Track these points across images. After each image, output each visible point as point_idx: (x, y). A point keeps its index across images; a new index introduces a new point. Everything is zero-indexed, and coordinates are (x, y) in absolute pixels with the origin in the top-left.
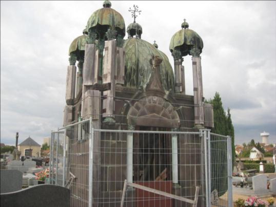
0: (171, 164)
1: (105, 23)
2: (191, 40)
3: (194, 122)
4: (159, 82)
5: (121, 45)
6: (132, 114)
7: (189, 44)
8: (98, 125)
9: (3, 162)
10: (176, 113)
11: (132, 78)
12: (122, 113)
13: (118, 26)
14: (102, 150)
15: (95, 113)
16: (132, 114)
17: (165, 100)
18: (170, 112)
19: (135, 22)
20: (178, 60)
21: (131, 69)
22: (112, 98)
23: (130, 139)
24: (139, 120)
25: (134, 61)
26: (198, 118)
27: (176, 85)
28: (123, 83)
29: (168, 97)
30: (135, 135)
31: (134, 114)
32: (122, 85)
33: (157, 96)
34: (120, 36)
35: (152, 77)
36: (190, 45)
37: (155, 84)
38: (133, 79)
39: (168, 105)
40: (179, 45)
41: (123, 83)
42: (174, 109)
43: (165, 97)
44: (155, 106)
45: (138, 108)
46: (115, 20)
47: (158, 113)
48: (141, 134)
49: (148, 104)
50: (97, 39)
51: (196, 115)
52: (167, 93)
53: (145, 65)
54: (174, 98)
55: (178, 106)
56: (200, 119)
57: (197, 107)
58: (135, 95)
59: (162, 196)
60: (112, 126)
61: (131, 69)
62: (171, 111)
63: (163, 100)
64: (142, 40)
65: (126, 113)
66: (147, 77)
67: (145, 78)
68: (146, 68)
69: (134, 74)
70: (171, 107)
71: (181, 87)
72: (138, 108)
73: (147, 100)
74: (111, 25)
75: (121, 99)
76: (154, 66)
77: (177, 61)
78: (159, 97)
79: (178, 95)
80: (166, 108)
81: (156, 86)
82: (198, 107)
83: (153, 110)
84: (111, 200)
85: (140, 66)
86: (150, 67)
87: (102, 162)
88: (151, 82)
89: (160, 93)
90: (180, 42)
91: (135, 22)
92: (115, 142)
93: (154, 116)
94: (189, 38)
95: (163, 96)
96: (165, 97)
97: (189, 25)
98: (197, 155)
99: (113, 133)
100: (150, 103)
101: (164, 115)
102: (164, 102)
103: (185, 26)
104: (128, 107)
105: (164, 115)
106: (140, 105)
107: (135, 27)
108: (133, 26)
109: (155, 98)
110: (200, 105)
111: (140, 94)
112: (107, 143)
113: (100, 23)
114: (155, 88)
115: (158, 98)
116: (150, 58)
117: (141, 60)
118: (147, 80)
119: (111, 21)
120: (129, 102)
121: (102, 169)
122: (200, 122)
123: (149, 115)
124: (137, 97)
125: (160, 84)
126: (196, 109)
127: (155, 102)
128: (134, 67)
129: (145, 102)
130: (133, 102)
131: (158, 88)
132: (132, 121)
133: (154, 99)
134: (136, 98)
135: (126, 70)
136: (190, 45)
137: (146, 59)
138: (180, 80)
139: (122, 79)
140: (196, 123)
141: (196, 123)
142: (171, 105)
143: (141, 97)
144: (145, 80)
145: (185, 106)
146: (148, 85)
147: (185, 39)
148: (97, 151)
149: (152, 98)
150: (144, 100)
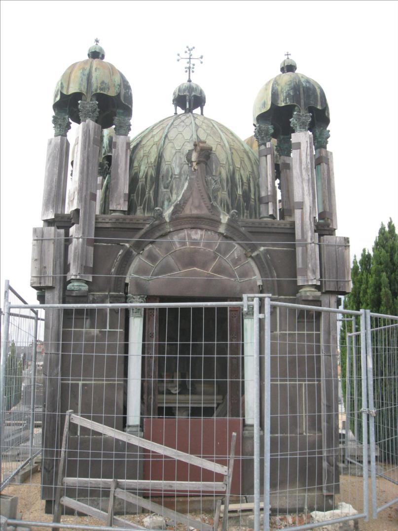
0: (243, 377)
1: (73, 89)
2: (288, 95)
3: (296, 282)
4: (205, 196)
5: (123, 132)
6: (136, 272)
7: (283, 104)
8: (56, 297)
9: (37, 426)
10: (253, 264)
11: (147, 196)
12: (113, 270)
13: (99, 91)
14: (65, 348)
15: (45, 273)
16: (136, 272)
17: (221, 234)
18: (235, 262)
19: (189, 81)
20: (265, 144)
21: (146, 178)
22: (81, 240)
23: (136, 326)
24: (156, 283)
25: (153, 160)
26: (305, 274)
27: (260, 200)
28: (126, 209)
29: (226, 230)
30: (147, 314)
31: (142, 270)
32: (123, 212)
33: (201, 229)
34: (121, 111)
35: (190, 187)
36: (294, 113)
37: (197, 203)
38: (149, 198)
39: (229, 248)
40: (264, 111)
41: (126, 209)
42: (246, 256)
43: (222, 229)
44: (196, 251)
45: (152, 258)
46: (94, 80)
47: (204, 266)
48: (162, 311)
49: (178, 246)
50: (274, 136)
51: (299, 264)
52: (225, 219)
53: (174, 163)
54: (243, 229)
55: (254, 248)
56: (310, 274)
57: (300, 245)
58: (142, 232)
59: (89, 418)
60: (82, 298)
61: (146, 178)
62: (239, 259)
63: (217, 236)
64: (205, 118)
65: (123, 267)
66: (178, 190)
67: (174, 192)
68: (177, 171)
69: (151, 188)
70: (237, 250)
71: (270, 204)
72: (152, 258)
73: (176, 238)
74: (84, 91)
75: (111, 242)
76: (194, 164)
77: (263, 147)
78: (207, 230)
79: (266, 223)
80: (225, 254)
81: (198, 207)
82: (305, 245)
83: (190, 259)
84: (94, 455)
85: (164, 167)
86: (186, 167)
87: (64, 373)
88: (185, 201)
89: (208, 222)
90: (264, 104)
91: (189, 81)
92: (95, 331)
93: (195, 273)
94: (282, 92)
95: (218, 227)
96: (222, 229)
97: (298, 66)
98: (311, 359)
99: (91, 312)
100: (184, 244)
101: (220, 270)
102: (219, 241)
103: (289, 68)
104: (127, 259)
105: (220, 270)
106: (157, 251)
107: (185, 90)
108: (179, 90)
109: (197, 235)
110: (309, 241)
111: (153, 229)
112: (78, 336)
113: (65, 92)
114: (195, 212)
115: (203, 232)
116: (190, 147)
117: (167, 156)
118: (178, 195)
119: (85, 83)
120: (127, 245)
121: (64, 387)
122: (307, 281)
123: (180, 273)
124: (146, 235)
125: (207, 200)
126: (299, 250)
127: (195, 243)
128: (152, 172)
129: (172, 243)
130: (139, 246)
131: (204, 212)
132: (138, 285)
133: (194, 237)
134: (145, 235)
135: (134, 180)
136: (294, 113)
137: (179, 151)
138: (270, 188)
139: (122, 201)
140: (300, 283)
141: (300, 283)
142: (237, 246)
143: (158, 234)
144: (174, 197)
145: (274, 245)
146: (178, 208)
147: (275, 95)
148: (53, 352)
149: (189, 236)
150: (168, 239)
